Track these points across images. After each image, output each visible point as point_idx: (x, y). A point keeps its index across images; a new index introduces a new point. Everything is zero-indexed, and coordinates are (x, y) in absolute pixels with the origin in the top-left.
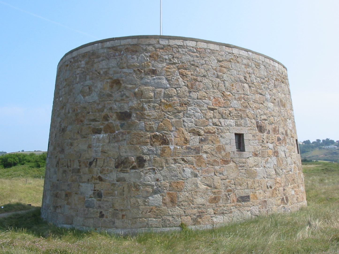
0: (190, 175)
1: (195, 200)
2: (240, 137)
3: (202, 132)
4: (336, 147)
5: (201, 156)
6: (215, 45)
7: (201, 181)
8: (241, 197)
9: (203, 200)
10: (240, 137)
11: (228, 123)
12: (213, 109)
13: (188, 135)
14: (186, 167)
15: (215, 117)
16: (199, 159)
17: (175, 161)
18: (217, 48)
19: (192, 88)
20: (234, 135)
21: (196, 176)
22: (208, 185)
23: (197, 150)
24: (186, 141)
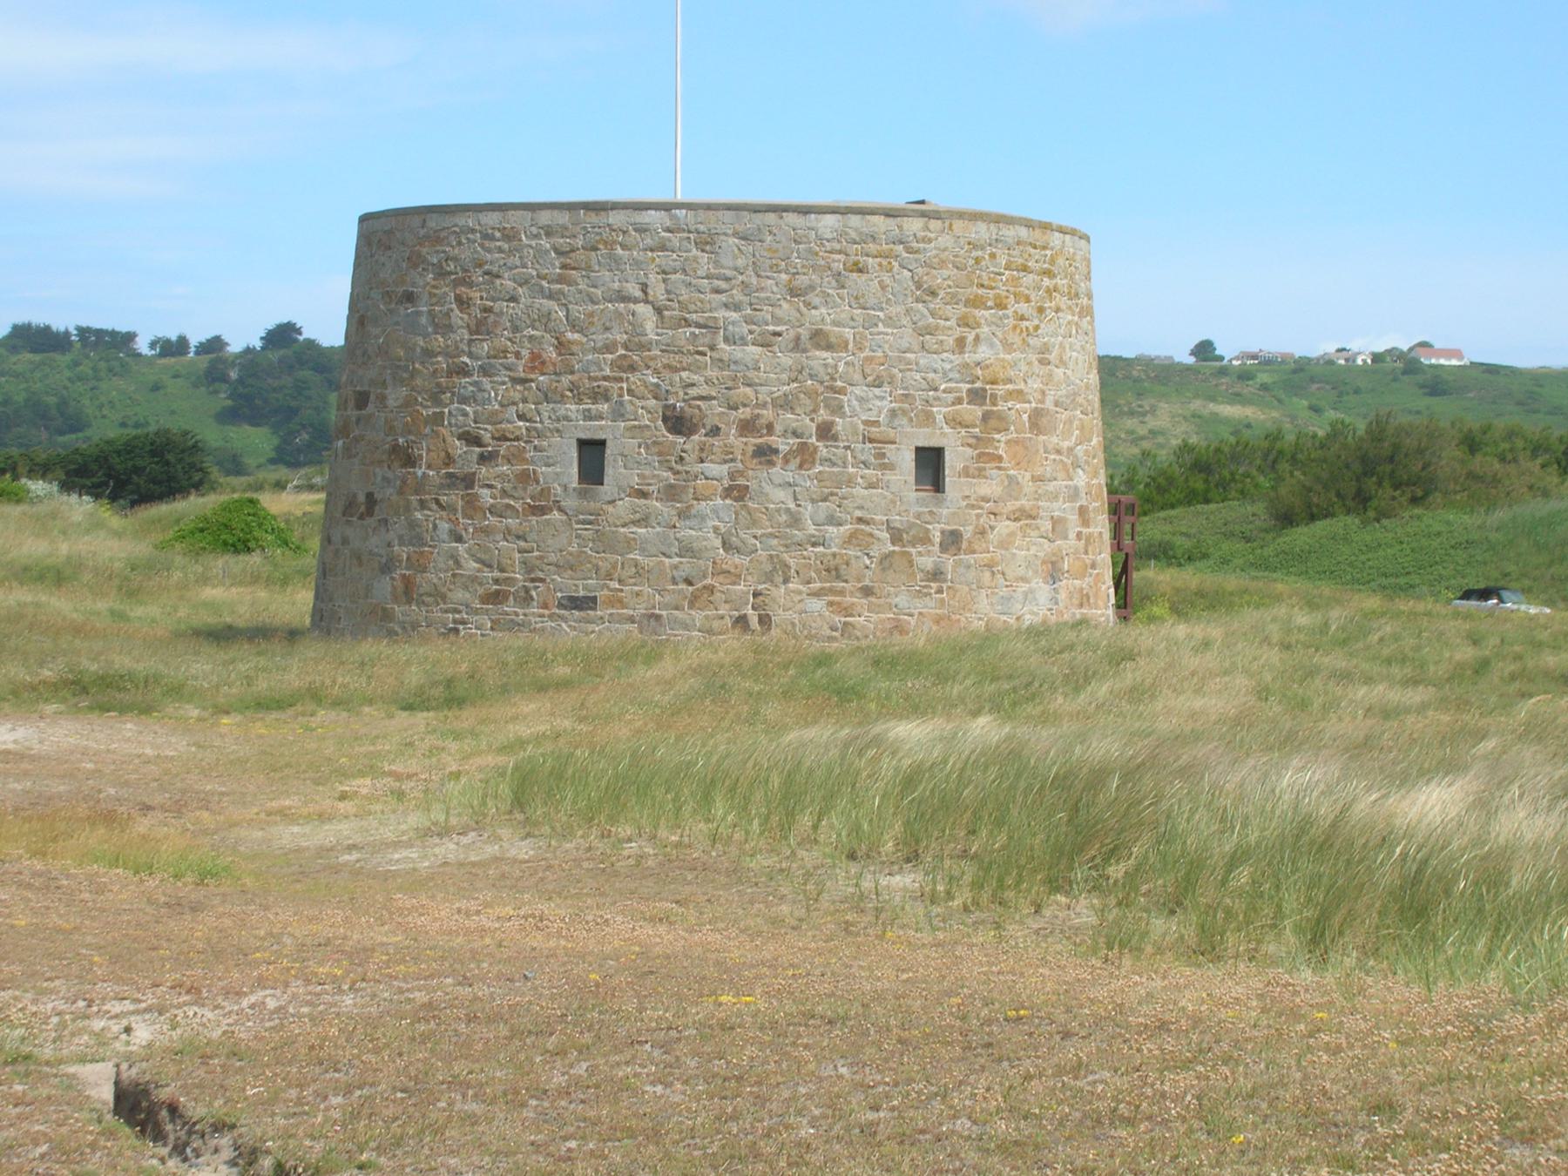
0: (445, 537)
1: (449, 594)
2: (592, 453)
3: (487, 437)
4: (404, 858)
5: (476, 496)
6: (556, 212)
7: (468, 551)
8: (571, 599)
9: (468, 595)
10: (592, 453)
11: (562, 412)
12: (524, 381)
13: (459, 448)
14: (441, 518)
15: (525, 401)
16: (472, 504)
17: (423, 505)
18: (563, 218)
19: (480, 328)
20: (574, 454)
21: (459, 539)
22: (483, 562)
23: (469, 481)
24: (449, 460)
